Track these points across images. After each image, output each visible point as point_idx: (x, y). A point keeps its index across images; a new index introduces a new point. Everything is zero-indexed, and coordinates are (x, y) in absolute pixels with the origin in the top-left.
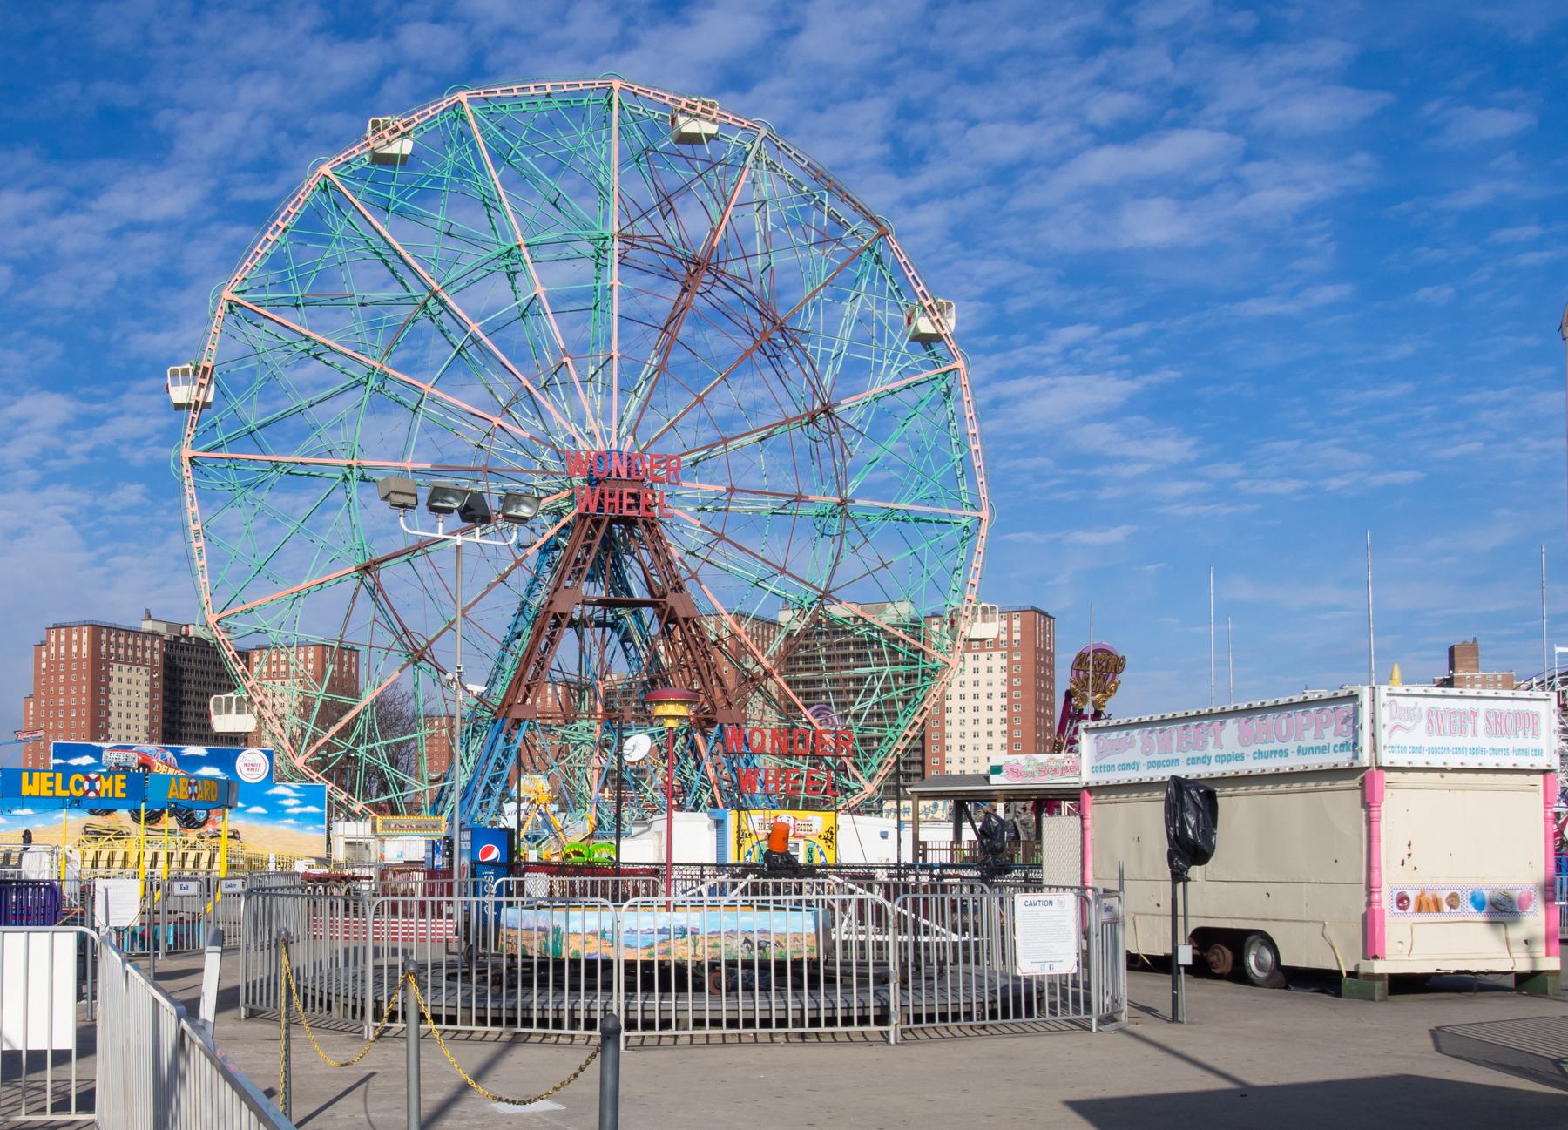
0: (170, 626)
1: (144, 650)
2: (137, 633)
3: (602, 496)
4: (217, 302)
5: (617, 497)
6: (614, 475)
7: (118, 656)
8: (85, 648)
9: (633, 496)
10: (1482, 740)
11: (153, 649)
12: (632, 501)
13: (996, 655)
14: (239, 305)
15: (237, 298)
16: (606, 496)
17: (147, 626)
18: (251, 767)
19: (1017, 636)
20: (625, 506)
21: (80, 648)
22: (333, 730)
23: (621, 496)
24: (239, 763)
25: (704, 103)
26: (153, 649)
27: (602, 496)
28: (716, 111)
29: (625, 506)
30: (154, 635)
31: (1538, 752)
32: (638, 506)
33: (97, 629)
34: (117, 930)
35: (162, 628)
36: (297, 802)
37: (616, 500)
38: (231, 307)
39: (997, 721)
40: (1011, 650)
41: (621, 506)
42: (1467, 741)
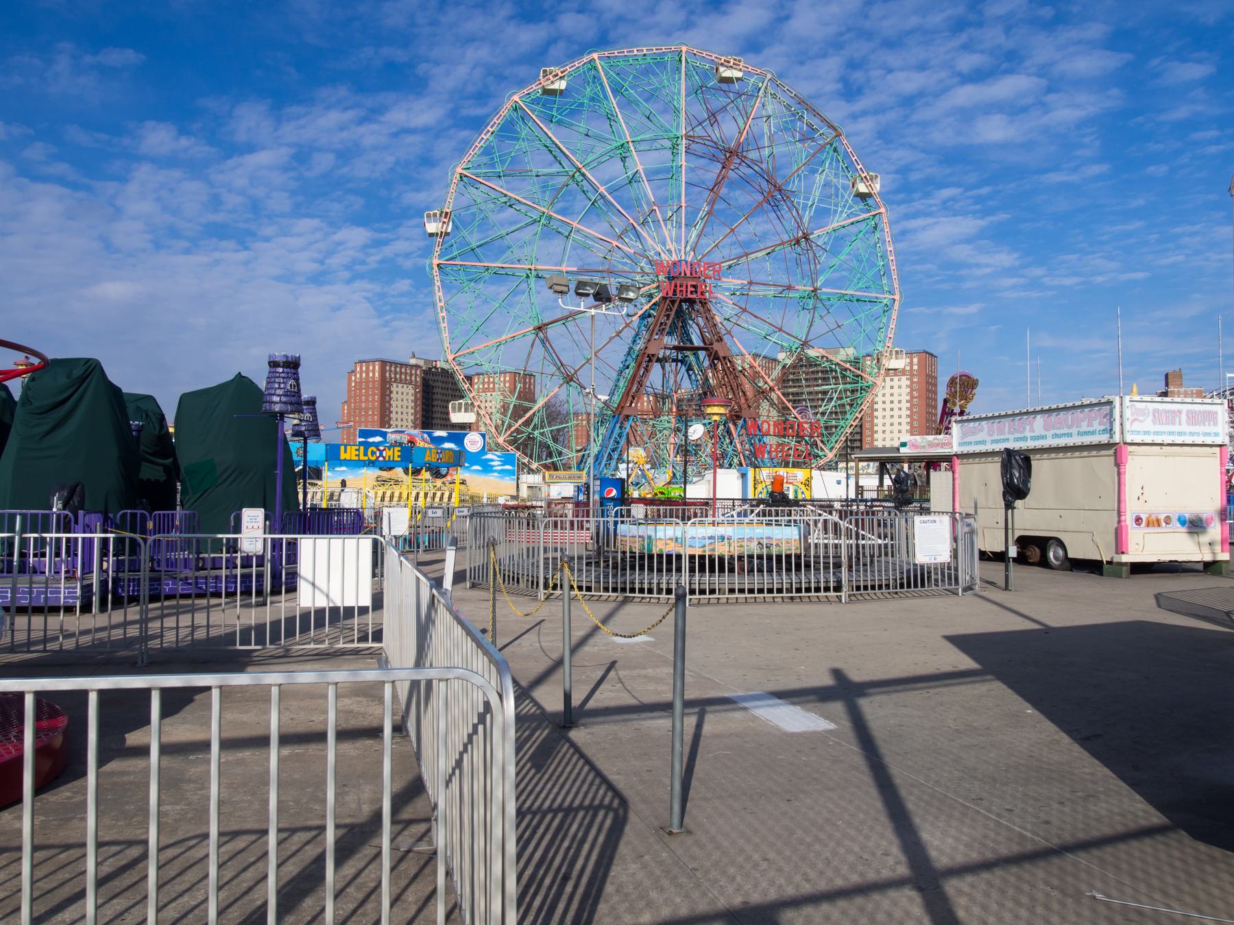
0: (426, 361)
1: (411, 375)
2: (406, 365)
3: (676, 286)
4: (453, 174)
5: (684, 287)
6: (683, 274)
7: (406, 380)
8: (377, 375)
9: (694, 286)
10: (1185, 428)
11: (416, 375)
12: (693, 289)
13: (904, 378)
14: (466, 176)
15: (465, 172)
16: (678, 286)
17: (413, 361)
18: (473, 443)
19: (915, 367)
20: (689, 292)
21: (374, 374)
22: (520, 422)
23: (687, 286)
24: (466, 441)
25: (735, 60)
26: (416, 375)
27: (676, 286)
28: (742, 64)
29: (689, 292)
30: (417, 366)
31: (1216, 434)
32: (696, 292)
33: (384, 363)
34: (396, 537)
35: (421, 363)
36: (499, 463)
37: (684, 289)
38: (461, 177)
39: (904, 416)
40: (912, 375)
41: (687, 292)
42: (1176, 428)
